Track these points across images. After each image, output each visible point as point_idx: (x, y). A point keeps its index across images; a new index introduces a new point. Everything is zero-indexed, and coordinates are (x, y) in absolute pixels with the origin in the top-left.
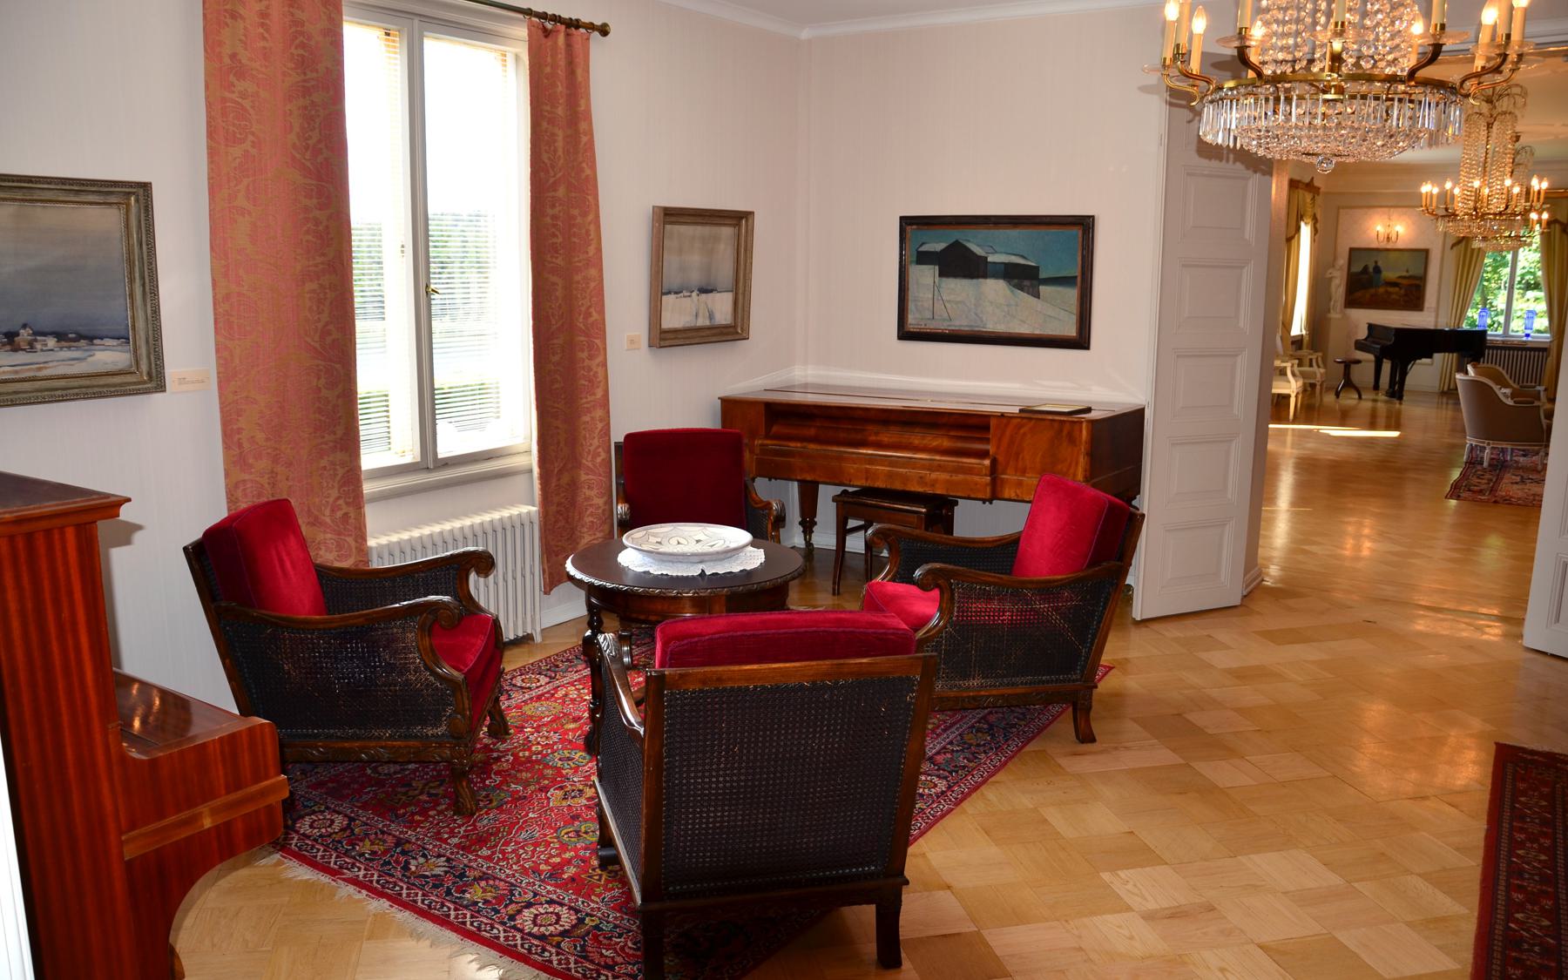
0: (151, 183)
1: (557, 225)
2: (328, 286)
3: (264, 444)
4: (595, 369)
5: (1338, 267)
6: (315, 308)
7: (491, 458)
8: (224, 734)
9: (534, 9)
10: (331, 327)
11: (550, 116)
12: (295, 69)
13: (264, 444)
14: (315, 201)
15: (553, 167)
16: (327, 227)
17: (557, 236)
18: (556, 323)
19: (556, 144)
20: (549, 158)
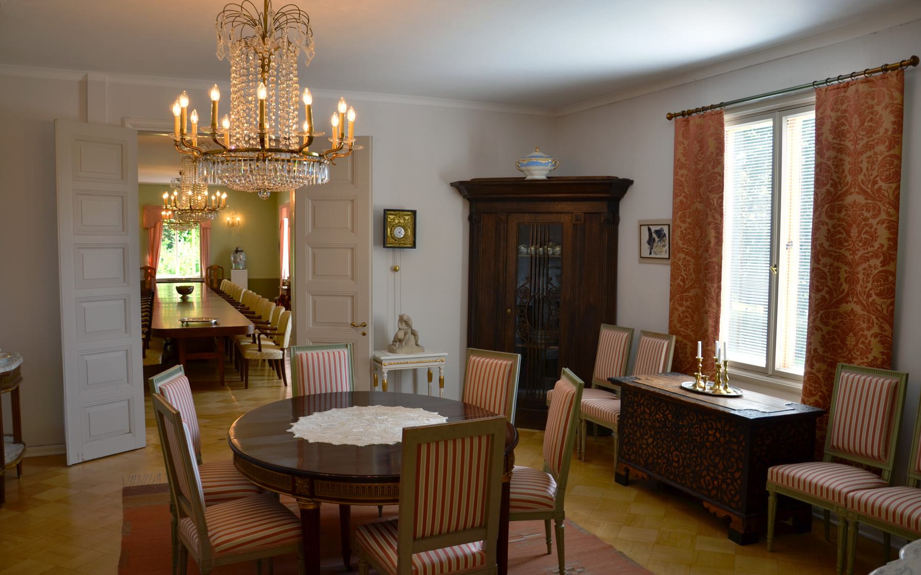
0: (639, 221)
1: (842, 225)
2: (873, 266)
3: (823, 354)
4: (869, 339)
5: (170, 241)
6: (865, 279)
7: (784, 378)
8: (595, 422)
9: (724, 102)
10: (872, 292)
11: (839, 147)
12: (867, 134)
13: (823, 354)
14: (871, 213)
15: (840, 184)
16: (876, 229)
17: (842, 233)
18: (688, 284)
19: (843, 167)
20: (838, 177)
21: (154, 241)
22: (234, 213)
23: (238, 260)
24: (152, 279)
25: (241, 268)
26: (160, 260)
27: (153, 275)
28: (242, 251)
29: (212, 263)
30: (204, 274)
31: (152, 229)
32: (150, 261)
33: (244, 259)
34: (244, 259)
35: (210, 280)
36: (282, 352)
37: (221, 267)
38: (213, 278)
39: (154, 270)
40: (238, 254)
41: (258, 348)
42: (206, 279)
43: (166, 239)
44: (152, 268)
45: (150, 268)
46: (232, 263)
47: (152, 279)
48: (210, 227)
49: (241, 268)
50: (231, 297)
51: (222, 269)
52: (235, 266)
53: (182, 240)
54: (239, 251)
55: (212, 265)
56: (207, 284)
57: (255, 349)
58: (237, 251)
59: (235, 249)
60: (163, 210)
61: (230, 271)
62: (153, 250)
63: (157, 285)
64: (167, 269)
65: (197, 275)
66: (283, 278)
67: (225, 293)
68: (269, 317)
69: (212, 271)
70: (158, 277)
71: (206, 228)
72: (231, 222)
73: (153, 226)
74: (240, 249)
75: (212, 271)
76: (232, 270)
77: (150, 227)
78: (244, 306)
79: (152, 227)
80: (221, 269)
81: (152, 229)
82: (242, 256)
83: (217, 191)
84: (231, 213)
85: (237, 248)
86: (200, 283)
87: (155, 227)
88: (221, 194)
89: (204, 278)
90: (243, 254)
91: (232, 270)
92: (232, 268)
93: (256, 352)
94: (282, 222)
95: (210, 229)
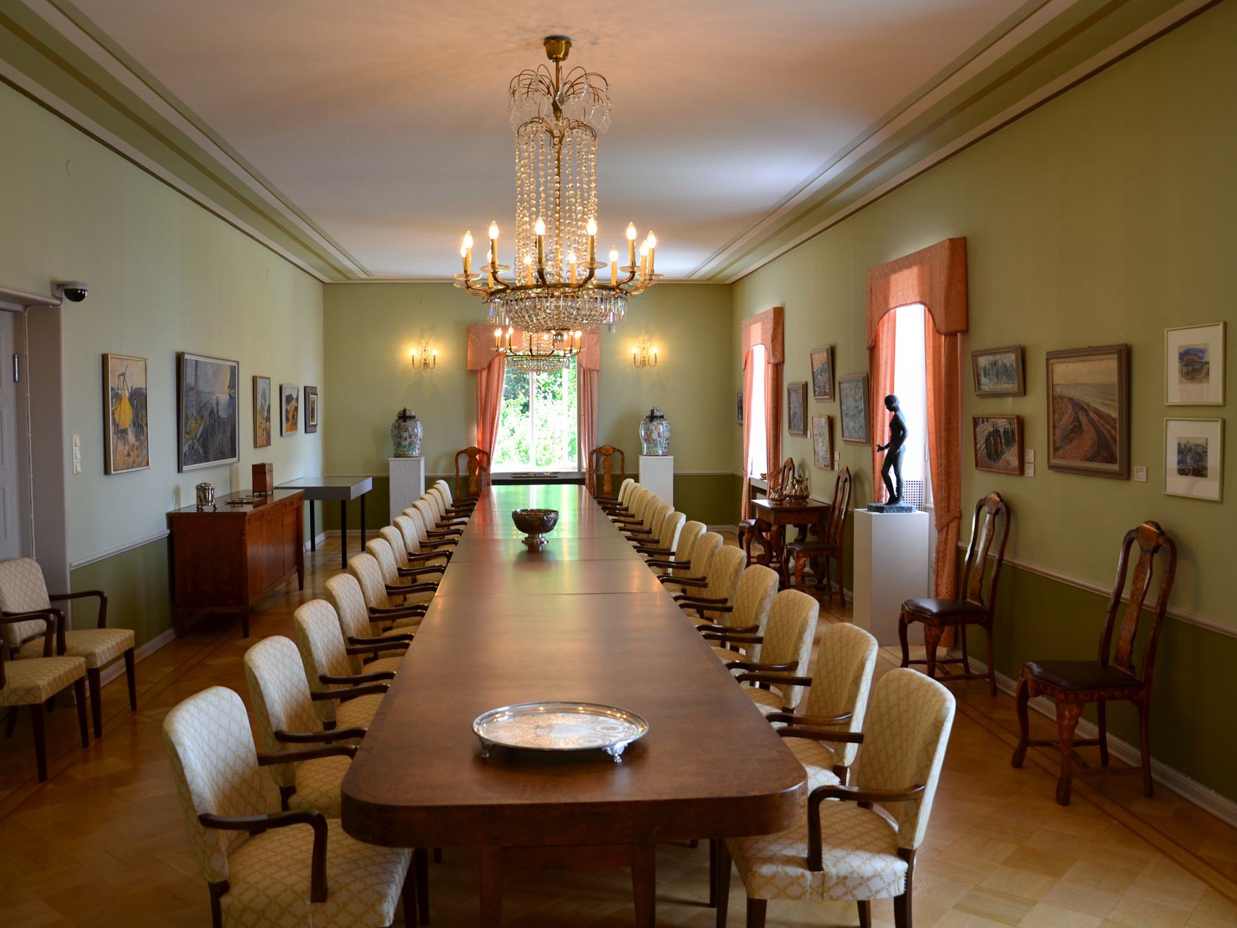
21: (487, 395)
22: (646, 338)
23: (655, 436)
24: (483, 473)
25: (660, 453)
26: (497, 443)
27: (485, 465)
28: (662, 417)
29: (600, 441)
30: (585, 464)
31: (484, 374)
32: (480, 438)
33: (667, 434)
34: (667, 434)
35: (598, 476)
36: (902, 866)
37: (619, 450)
38: (602, 472)
39: (487, 455)
40: (655, 423)
41: (802, 851)
42: (590, 475)
43: (521, 396)
44: (484, 452)
45: (479, 451)
46: (642, 441)
47: (483, 473)
48: (598, 368)
49: (660, 453)
50: (646, 527)
51: (622, 453)
52: (648, 448)
53: (550, 396)
54: (656, 417)
55: (601, 444)
56: (589, 489)
57: (790, 852)
58: (652, 418)
59: (649, 413)
60: (495, 327)
61: (638, 458)
62: (485, 415)
63: (495, 490)
64: (521, 449)
65: (568, 465)
66: (749, 476)
67: (631, 511)
68: (797, 650)
69: (602, 459)
70: (497, 467)
71: (591, 370)
72: (638, 358)
73: (485, 365)
74: (658, 414)
75: (602, 459)
76: (641, 458)
77: (479, 368)
78: (685, 566)
79: (484, 369)
80: (618, 455)
81: (484, 374)
82: (661, 428)
83: (626, 225)
84: (641, 339)
85: (652, 412)
86: (576, 486)
87: (489, 367)
88: (642, 237)
89: (584, 473)
90: (664, 422)
91: (641, 458)
92: (641, 453)
93: (800, 871)
94: (750, 354)
95: (597, 371)
